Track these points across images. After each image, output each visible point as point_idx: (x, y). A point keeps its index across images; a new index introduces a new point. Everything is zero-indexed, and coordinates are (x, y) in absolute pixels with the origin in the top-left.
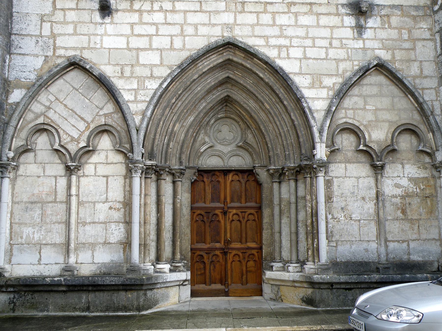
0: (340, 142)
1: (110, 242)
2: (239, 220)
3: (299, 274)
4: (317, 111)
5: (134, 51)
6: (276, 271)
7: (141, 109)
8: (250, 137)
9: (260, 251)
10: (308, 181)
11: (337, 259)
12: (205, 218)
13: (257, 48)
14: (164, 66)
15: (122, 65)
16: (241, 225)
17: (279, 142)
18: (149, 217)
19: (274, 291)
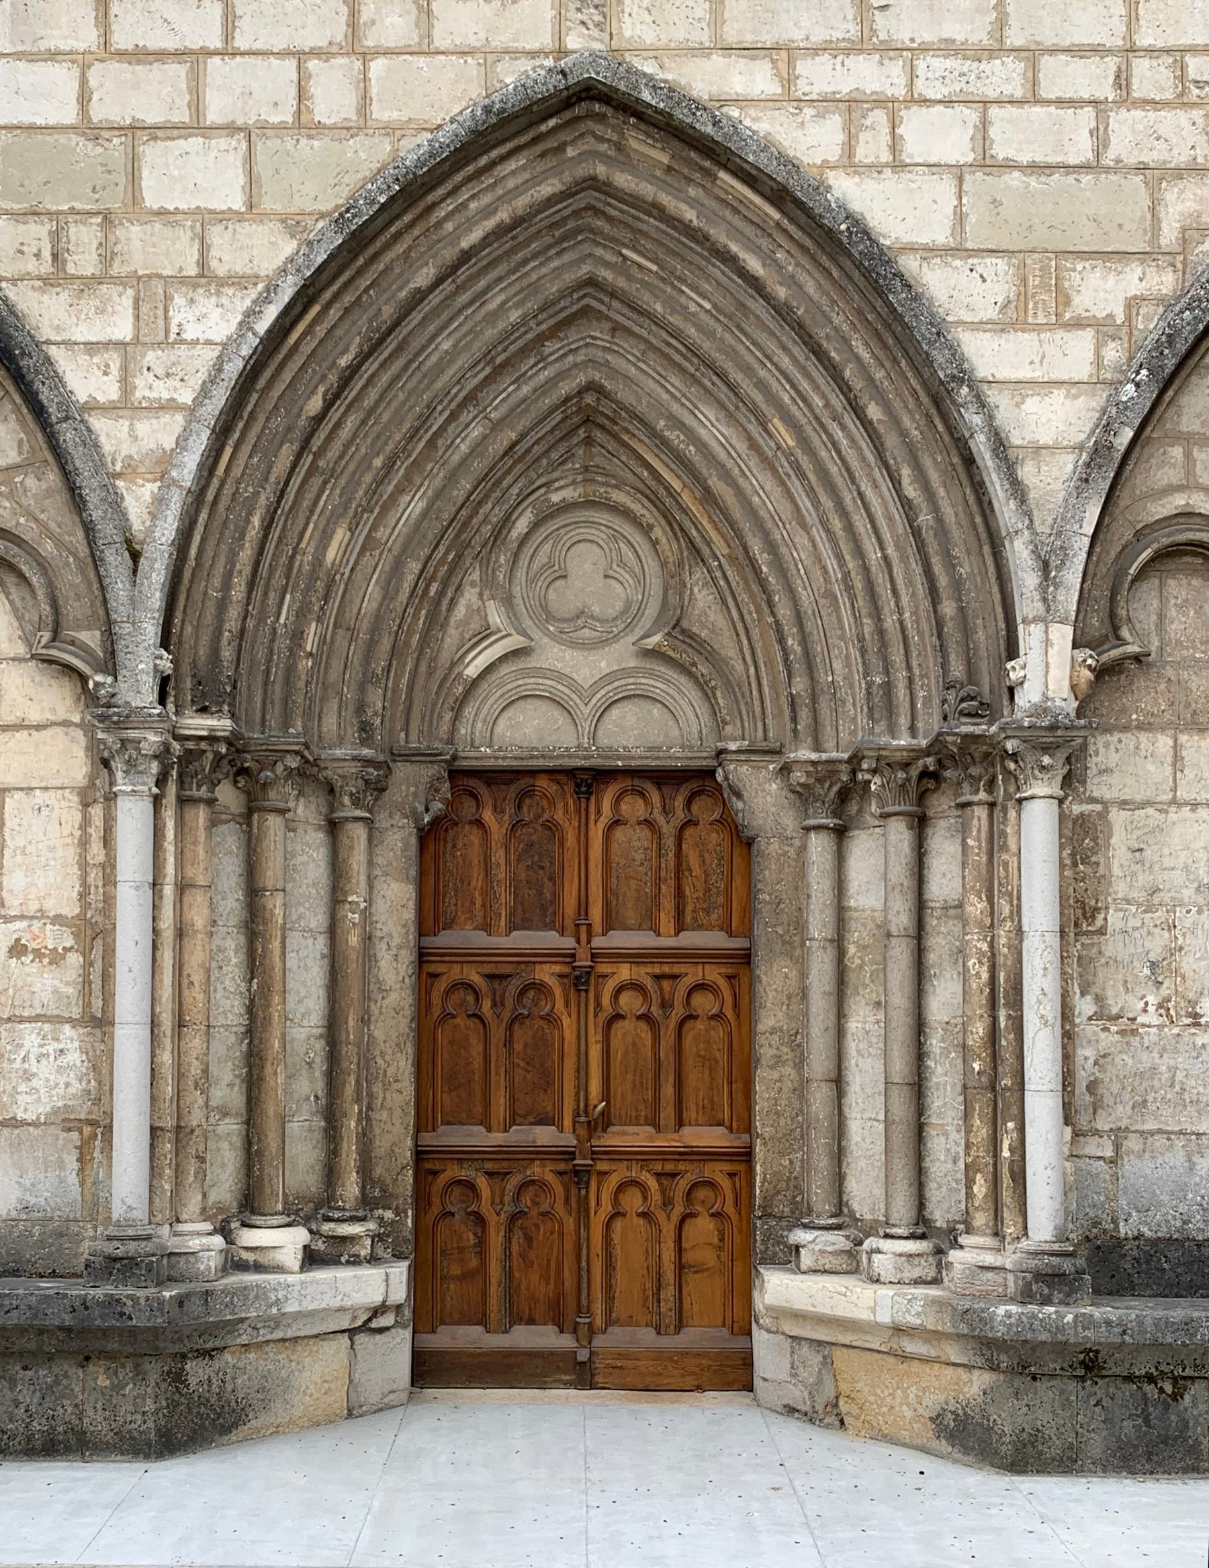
0: (1154, 617)
1: (14, 1118)
2: (646, 1017)
3: (921, 1291)
4: (1038, 449)
5: (115, 140)
6: (815, 1271)
7: (153, 446)
8: (700, 604)
9: (741, 1168)
10: (975, 822)
11: (1117, 1226)
12: (487, 1005)
13: (735, 113)
14: (263, 218)
15: (59, 213)
16: (656, 1039)
17: (842, 628)
18: (200, 997)
19: (803, 1374)
